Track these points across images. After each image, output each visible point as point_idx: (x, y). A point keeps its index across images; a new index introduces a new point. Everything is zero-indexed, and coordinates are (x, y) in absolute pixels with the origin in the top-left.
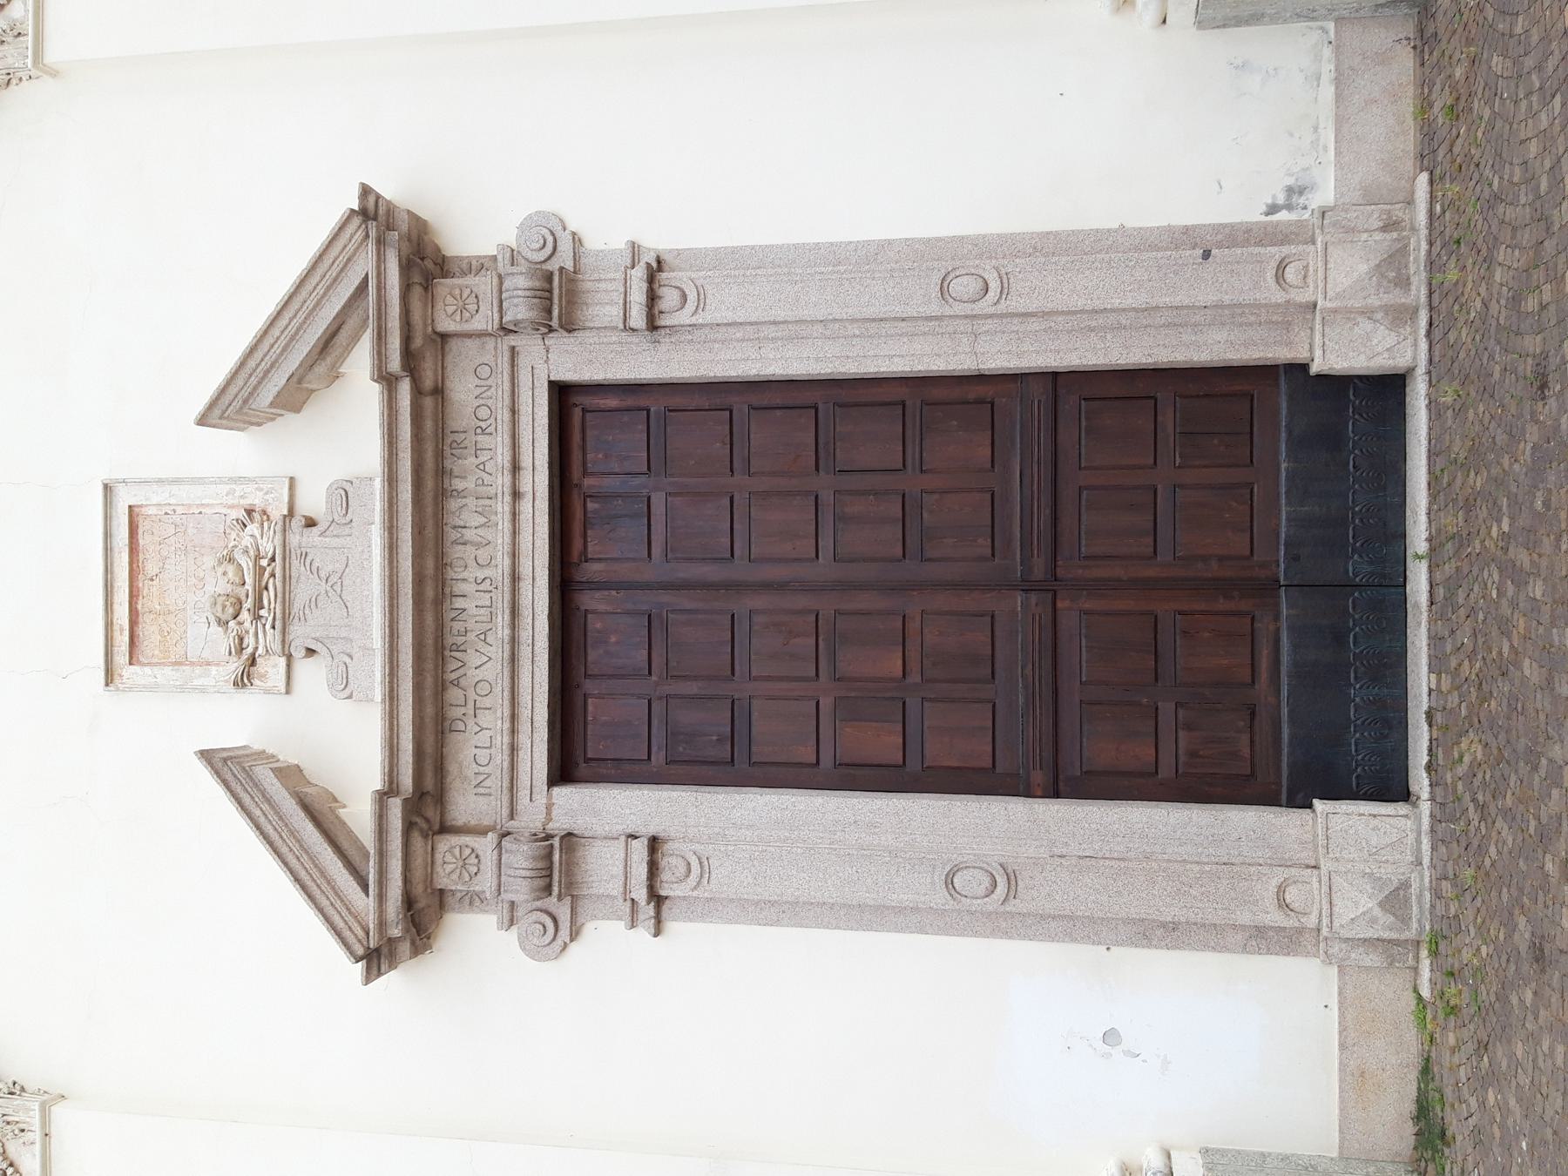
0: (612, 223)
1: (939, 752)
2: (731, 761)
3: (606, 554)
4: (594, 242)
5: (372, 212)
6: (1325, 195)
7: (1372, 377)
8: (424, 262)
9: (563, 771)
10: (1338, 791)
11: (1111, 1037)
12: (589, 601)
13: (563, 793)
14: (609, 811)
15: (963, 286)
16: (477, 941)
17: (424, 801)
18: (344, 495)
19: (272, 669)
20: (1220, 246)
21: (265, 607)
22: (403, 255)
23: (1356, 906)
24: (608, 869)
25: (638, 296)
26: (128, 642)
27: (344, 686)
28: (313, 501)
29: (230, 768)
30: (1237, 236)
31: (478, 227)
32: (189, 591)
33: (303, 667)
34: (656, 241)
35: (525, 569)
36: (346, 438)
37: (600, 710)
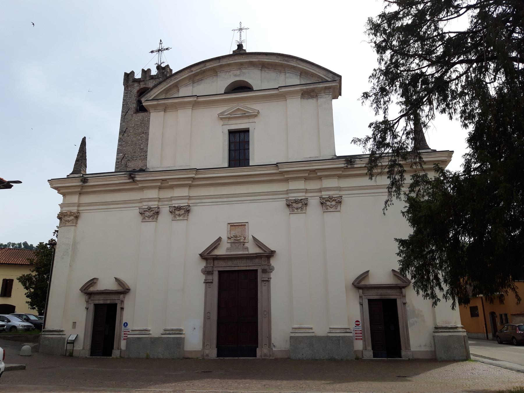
6: (274, 349)
11: (195, 328)
16: (203, 264)
20: (194, 178)
21: (237, 241)
22: (270, 254)
25: (265, 279)
26: (232, 225)
27: (228, 249)
28: (246, 245)
29: (220, 239)
32: (237, 232)
33: (229, 244)
35: (236, 262)
36: (253, 249)
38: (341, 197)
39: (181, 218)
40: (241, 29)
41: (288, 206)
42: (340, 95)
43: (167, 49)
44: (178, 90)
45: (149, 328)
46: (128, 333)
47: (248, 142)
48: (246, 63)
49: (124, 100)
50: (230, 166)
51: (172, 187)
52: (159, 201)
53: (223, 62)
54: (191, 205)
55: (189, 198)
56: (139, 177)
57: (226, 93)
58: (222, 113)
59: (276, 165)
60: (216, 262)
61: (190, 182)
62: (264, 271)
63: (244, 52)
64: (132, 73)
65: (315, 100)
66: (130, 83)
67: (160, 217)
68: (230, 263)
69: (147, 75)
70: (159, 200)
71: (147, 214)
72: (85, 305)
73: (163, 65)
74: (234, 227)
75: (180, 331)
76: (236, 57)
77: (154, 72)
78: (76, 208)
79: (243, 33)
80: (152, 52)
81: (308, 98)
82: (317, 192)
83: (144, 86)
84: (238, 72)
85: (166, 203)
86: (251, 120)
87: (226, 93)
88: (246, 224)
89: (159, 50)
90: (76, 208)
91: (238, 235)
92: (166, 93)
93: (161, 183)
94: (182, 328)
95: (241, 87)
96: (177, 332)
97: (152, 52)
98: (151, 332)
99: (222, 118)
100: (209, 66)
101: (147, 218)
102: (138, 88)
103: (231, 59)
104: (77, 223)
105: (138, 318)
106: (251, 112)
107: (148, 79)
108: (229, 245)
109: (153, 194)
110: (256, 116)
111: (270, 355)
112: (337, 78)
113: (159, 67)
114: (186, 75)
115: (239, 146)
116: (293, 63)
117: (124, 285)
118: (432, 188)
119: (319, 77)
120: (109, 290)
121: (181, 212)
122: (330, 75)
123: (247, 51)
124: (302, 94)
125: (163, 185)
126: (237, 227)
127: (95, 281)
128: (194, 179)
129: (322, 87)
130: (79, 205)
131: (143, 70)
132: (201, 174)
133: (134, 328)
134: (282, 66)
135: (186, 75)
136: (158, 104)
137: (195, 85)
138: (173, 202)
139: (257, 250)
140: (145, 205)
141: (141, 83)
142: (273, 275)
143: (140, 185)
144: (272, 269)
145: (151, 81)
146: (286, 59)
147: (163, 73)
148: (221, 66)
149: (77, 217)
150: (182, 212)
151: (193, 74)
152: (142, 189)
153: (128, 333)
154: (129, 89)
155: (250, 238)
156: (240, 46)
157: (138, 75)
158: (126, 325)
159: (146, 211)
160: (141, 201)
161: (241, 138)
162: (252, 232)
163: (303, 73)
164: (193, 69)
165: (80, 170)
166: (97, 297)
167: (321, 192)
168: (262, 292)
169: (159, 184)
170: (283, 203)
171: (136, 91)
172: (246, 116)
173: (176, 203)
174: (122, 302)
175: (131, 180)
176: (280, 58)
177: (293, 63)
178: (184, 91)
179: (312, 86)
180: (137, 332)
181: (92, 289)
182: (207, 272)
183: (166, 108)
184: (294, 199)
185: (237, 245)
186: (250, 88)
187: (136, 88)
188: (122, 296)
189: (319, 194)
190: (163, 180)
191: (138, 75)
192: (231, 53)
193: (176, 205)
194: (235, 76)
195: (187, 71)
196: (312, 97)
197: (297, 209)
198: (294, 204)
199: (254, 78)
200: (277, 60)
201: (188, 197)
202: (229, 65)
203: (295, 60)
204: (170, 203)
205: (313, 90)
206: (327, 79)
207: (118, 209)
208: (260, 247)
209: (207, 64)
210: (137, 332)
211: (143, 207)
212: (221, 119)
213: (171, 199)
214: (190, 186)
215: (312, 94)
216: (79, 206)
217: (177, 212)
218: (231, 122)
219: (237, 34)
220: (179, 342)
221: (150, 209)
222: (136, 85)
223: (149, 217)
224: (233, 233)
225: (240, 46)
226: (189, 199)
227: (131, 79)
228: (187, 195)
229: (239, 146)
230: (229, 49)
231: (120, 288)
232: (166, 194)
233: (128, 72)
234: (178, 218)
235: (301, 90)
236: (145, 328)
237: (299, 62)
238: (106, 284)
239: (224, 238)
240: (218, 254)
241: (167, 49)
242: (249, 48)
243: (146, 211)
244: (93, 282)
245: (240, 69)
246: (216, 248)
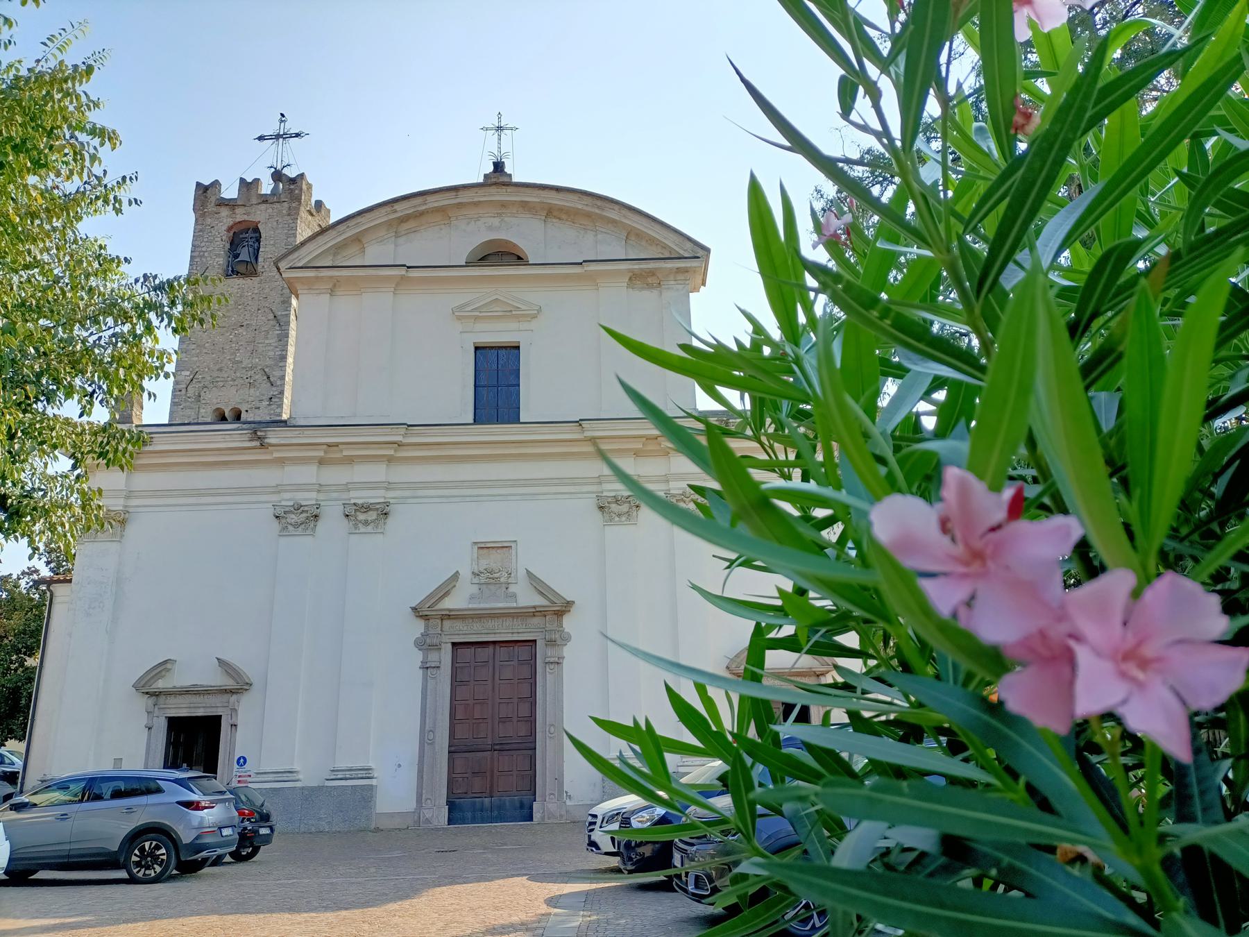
0: (568, 652)
1: (458, 727)
2: (456, 682)
3: (502, 652)
4: (565, 649)
5: (569, 604)
6: (568, 803)
7: (532, 700)
8: (560, 614)
9: (454, 644)
10: (450, 811)
11: (400, 766)
12: (491, 647)
13: (450, 646)
14: (446, 654)
15: (552, 729)
16: (419, 627)
17: (448, 616)
18: (514, 596)
19: (476, 580)
20: (400, 440)
21: (489, 580)
22: (562, 609)
23: (428, 814)
24: (433, 657)
25: (552, 660)
26: (483, 548)
27: (472, 598)
28: (512, 589)
29: (456, 576)
30: (561, 784)
31: (568, 623)
32: (492, 561)
33: (476, 587)
34: (565, 663)
35: (490, 624)
36: (527, 598)
37: (469, 652)
38: (388, 504)
39: (369, 529)
40: (500, 128)
41: (601, 508)
42: (704, 284)
43: (297, 135)
44: (363, 250)
45: (296, 767)
46: (249, 779)
47: (517, 373)
48: (513, 203)
49: (195, 247)
50: (476, 421)
51: (350, 460)
52: (319, 491)
53: (464, 197)
54: (131, 510)
55: (389, 486)
56: (274, 436)
57: (468, 264)
58: (461, 308)
59: (579, 422)
60: (447, 623)
61: (392, 452)
62: (551, 643)
63: (506, 179)
64: (216, 184)
65: (656, 292)
66: (211, 207)
67: (321, 524)
68: (477, 626)
69: (253, 192)
70: (320, 488)
71: (293, 518)
72: (144, 720)
73: (291, 173)
74: (485, 551)
75: (367, 773)
76: (493, 190)
77: (267, 187)
78: (122, 501)
79: (506, 135)
80: (261, 138)
81: (643, 289)
82: (592, 484)
83: (246, 218)
84: (496, 221)
85: (335, 495)
86: (524, 326)
87: (468, 264)
88: (513, 545)
89: (278, 137)
90: (122, 501)
91: (493, 566)
92: (335, 255)
93: (326, 452)
94: (371, 764)
95: (499, 255)
96: (363, 774)
97: (261, 138)
98: (300, 777)
99: (459, 314)
100: (433, 202)
101: (290, 528)
102: (230, 222)
103: (481, 191)
104: (122, 536)
105: (270, 748)
106: (523, 307)
107: (254, 201)
108: (475, 589)
109: (307, 474)
110: (534, 317)
111: (561, 816)
112: (700, 253)
113: (277, 176)
114: (381, 217)
115: (497, 382)
116: (613, 214)
117: (238, 674)
118: (44, 413)
119: (665, 247)
120: (202, 686)
121: (369, 514)
122: (689, 245)
123: (515, 179)
124: (630, 279)
125: (329, 457)
126: (494, 551)
127: (169, 666)
128: (400, 445)
129: (671, 269)
130: (129, 495)
131: (242, 180)
132: (418, 435)
133: (262, 769)
134: (588, 215)
135: (381, 217)
136: (317, 278)
137: (401, 240)
138: (353, 494)
139: (539, 601)
140: (287, 499)
141: (239, 211)
142: (567, 651)
143: (276, 455)
144: (566, 639)
145: (263, 206)
146: (599, 203)
147: (292, 191)
148: (460, 206)
149: (123, 522)
150: (372, 515)
151: (398, 218)
152: (281, 462)
153: (249, 779)
154: (209, 221)
155: (522, 573)
156: (498, 166)
157: (230, 191)
158: (242, 761)
159: (290, 512)
160: (278, 489)
161: (501, 362)
162: (527, 559)
163: (632, 235)
164: (397, 206)
165: (130, 417)
166: (172, 700)
167: (600, 483)
168: (545, 686)
169: (321, 454)
170: (591, 503)
171: (225, 228)
172: (512, 314)
173: (360, 497)
174: (234, 710)
175: (257, 443)
176: (588, 200)
177: (613, 214)
178: (376, 252)
179: (652, 265)
180: (271, 777)
181: (161, 684)
182: (425, 645)
183: (335, 285)
184: (613, 494)
185: (492, 587)
186: (519, 258)
187: (225, 220)
188: (234, 697)
189: (594, 488)
190: (329, 445)
191: (230, 191)
192: (481, 180)
193: (360, 502)
194: (490, 228)
195: (383, 210)
196: (650, 287)
197: (619, 515)
198: (613, 506)
199: (525, 234)
200: (579, 204)
201: (317, 487)
202: (476, 204)
203: (616, 207)
204: (345, 496)
205: (652, 273)
206: (682, 252)
207: (177, 508)
208: (541, 593)
209: (430, 198)
210: (271, 777)
211: (284, 503)
212: (459, 318)
213: (347, 487)
214: (390, 460)
215: (650, 280)
216: (127, 497)
217: (361, 517)
218: (480, 326)
219: (492, 136)
220: (366, 796)
221: (298, 508)
222: (225, 212)
223: (296, 526)
224: (484, 564)
225: (498, 166)
226: (387, 489)
227: (213, 199)
228: (314, 481)
229: (497, 382)
230: (476, 172)
231: (229, 683)
232: (335, 475)
233: (207, 183)
234: (363, 529)
235: (629, 270)
236: (287, 768)
237: (625, 212)
238: (195, 670)
239: (466, 573)
240: (451, 607)
241: (297, 135)
242: (519, 172)
243: (290, 512)
244: (163, 667)
245: (499, 215)
246: (447, 594)
